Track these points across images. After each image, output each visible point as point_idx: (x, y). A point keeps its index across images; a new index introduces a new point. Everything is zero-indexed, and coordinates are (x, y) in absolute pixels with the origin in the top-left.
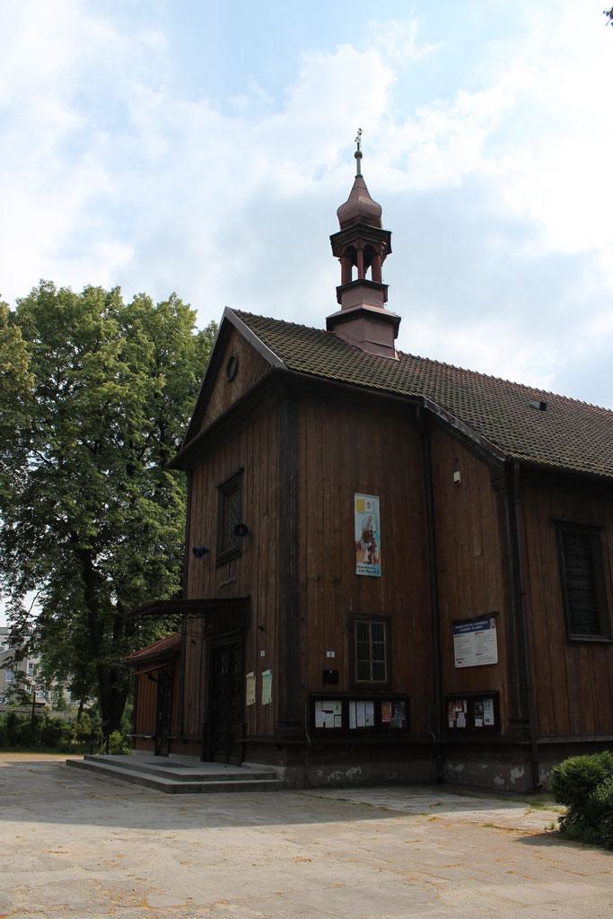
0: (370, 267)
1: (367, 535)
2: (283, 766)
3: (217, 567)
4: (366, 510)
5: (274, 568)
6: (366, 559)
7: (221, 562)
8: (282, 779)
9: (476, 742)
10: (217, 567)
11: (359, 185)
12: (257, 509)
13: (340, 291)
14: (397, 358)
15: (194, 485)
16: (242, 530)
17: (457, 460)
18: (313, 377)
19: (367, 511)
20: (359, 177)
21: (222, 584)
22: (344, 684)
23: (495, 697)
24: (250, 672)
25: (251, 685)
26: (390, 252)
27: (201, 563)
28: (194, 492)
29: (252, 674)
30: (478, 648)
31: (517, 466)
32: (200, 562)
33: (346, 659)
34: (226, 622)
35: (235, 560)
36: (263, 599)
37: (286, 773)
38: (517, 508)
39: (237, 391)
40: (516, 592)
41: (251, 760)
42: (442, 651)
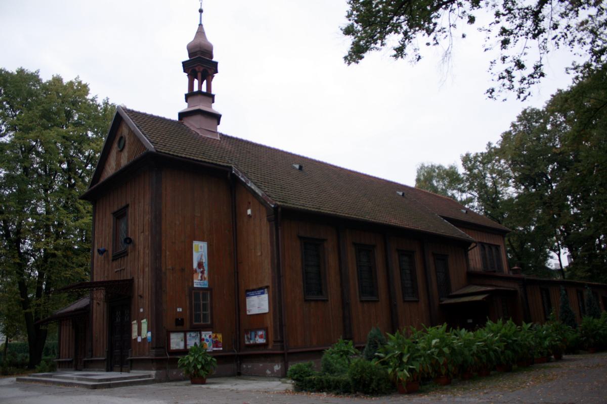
1: (200, 265)
2: (155, 370)
3: (113, 260)
4: (200, 250)
5: (147, 262)
6: (200, 278)
7: (115, 258)
8: (154, 378)
10: (113, 260)
11: (201, 32)
12: (137, 228)
13: (187, 97)
14: (219, 139)
16: (128, 241)
17: (250, 203)
18: (170, 156)
19: (200, 251)
20: (201, 25)
21: (116, 270)
22: (187, 325)
23: (266, 330)
24: (134, 320)
25: (135, 328)
26: (216, 72)
27: (103, 257)
28: (97, 215)
29: (135, 322)
30: (258, 304)
31: (280, 210)
32: (101, 257)
33: (188, 312)
34: (120, 297)
35: (124, 256)
36: (141, 280)
37: (156, 375)
38: (280, 231)
39: (124, 162)
40: (278, 276)
41: (135, 369)
42: (240, 306)
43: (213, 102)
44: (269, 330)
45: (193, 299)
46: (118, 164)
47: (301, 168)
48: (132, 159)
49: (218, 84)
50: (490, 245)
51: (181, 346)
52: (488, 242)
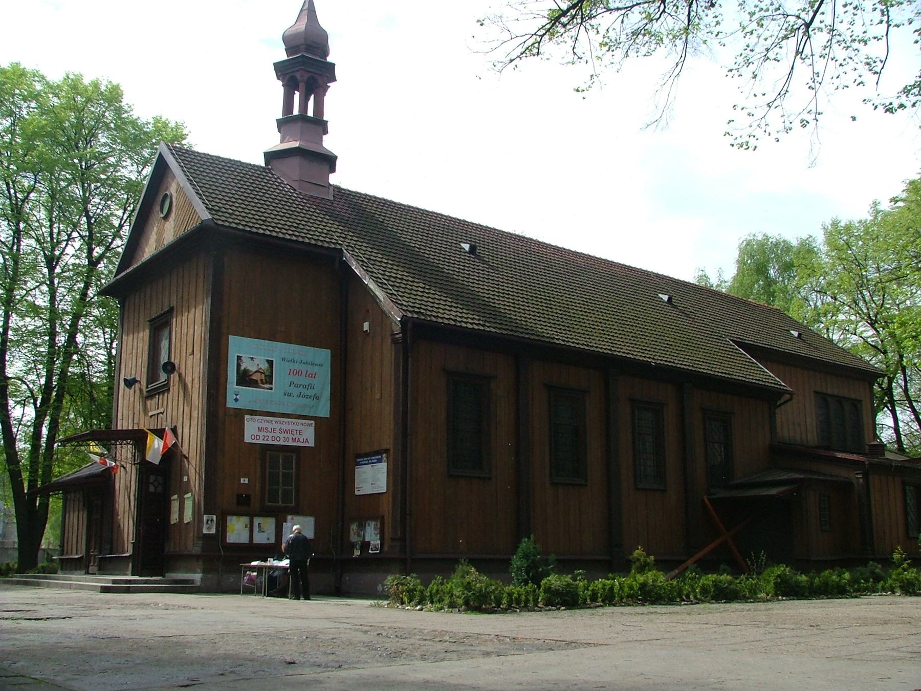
0: (312, 97)
7: (151, 395)
8: (199, 584)
9: (377, 563)
13: (281, 124)
15: (126, 317)
16: (170, 367)
25: (175, 506)
26: (334, 79)
29: (176, 497)
31: (410, 325)
33: (258, 488)
42: (346, 480)
43: (325, 132)
44: (388, 521)
45: (268, 464)
46: (158, 241)
47: (473, 249)
48: (181, 233)
49: (336, 102)
50: (839, 400)
51: (244, 539)
52: (836, 392)
